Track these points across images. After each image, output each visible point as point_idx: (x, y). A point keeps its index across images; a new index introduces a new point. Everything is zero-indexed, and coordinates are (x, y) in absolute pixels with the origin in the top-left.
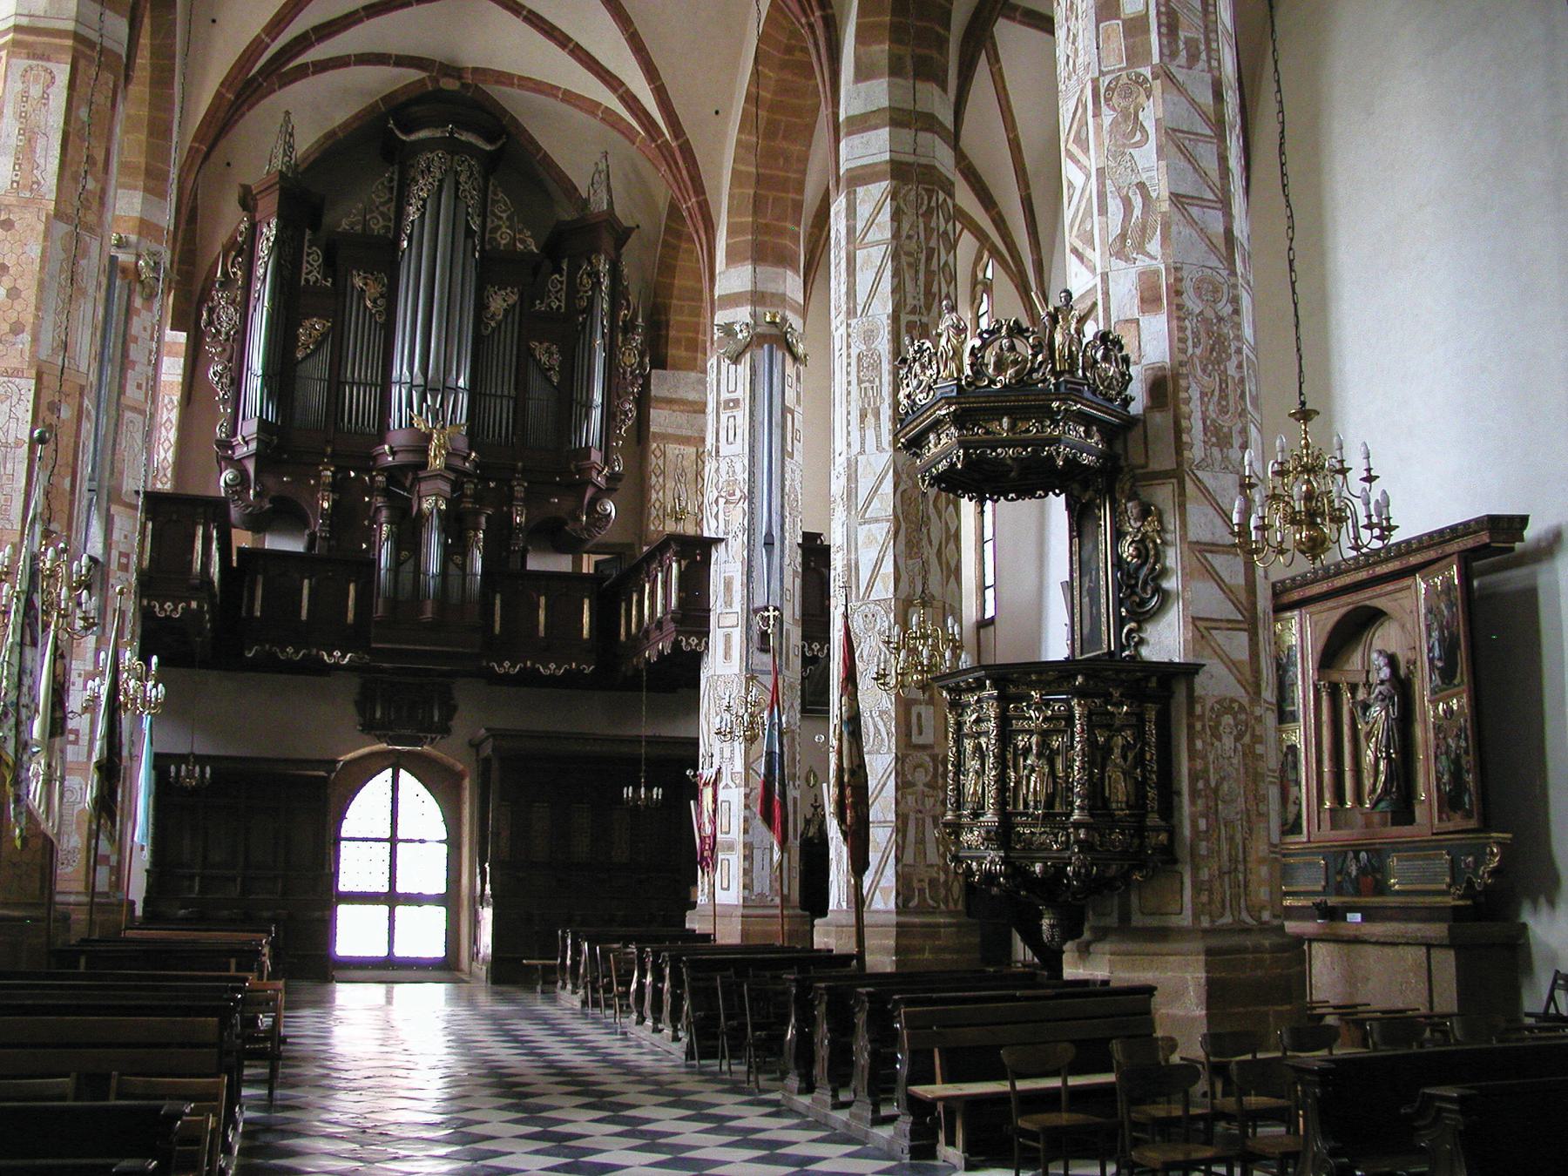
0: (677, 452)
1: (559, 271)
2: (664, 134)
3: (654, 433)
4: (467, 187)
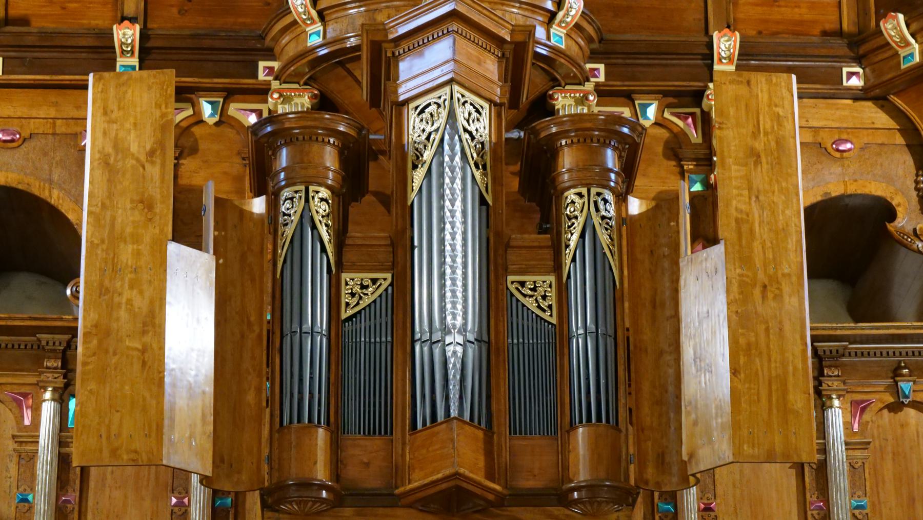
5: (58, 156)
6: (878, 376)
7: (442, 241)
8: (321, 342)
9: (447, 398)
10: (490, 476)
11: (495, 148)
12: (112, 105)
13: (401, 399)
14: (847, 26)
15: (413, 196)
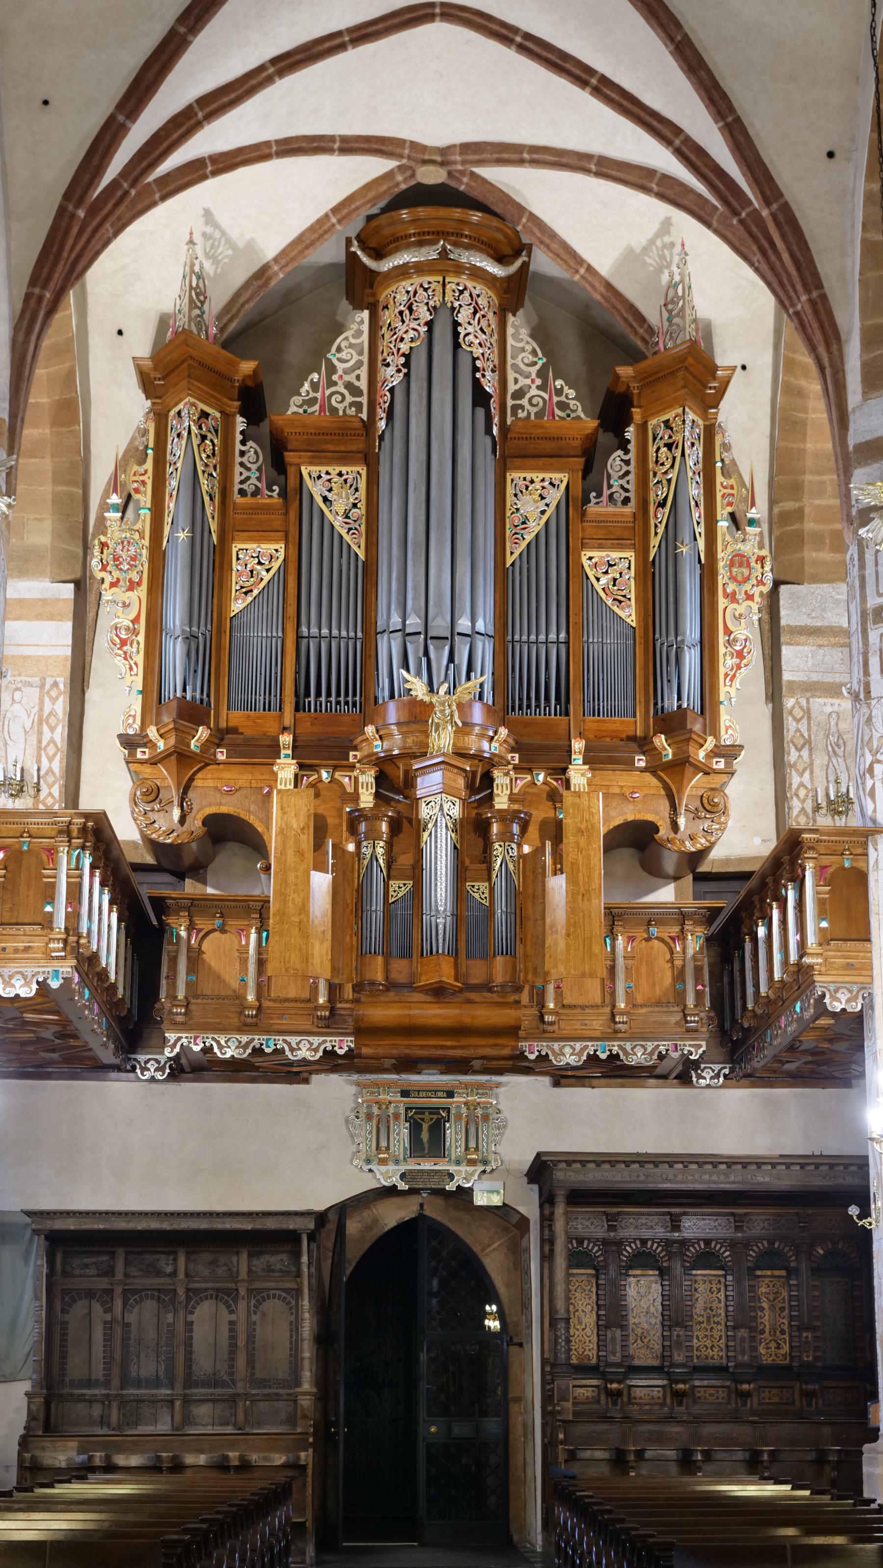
0: (828, 709)
1: (623, 445)
2: (750, 202)
3: (790, 683)
4: (470, 329)
5: (253, 798)
6: (640, 925)
7: (436, 869)
8: (380, 914)
9: (437, 940)
10: (456, 980)
11: (461, 820)
12: (285, 805)
13: (416, 942)
14: (639, 733)
15: (423, 845)
